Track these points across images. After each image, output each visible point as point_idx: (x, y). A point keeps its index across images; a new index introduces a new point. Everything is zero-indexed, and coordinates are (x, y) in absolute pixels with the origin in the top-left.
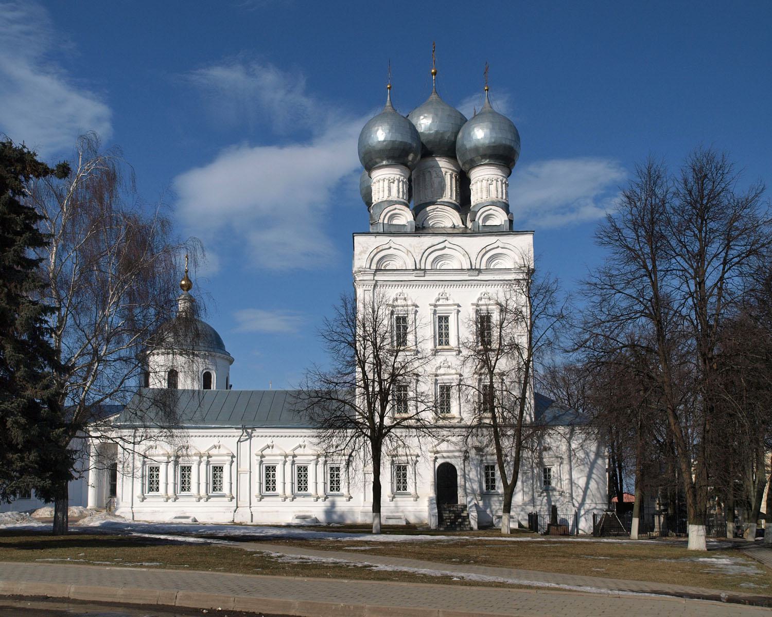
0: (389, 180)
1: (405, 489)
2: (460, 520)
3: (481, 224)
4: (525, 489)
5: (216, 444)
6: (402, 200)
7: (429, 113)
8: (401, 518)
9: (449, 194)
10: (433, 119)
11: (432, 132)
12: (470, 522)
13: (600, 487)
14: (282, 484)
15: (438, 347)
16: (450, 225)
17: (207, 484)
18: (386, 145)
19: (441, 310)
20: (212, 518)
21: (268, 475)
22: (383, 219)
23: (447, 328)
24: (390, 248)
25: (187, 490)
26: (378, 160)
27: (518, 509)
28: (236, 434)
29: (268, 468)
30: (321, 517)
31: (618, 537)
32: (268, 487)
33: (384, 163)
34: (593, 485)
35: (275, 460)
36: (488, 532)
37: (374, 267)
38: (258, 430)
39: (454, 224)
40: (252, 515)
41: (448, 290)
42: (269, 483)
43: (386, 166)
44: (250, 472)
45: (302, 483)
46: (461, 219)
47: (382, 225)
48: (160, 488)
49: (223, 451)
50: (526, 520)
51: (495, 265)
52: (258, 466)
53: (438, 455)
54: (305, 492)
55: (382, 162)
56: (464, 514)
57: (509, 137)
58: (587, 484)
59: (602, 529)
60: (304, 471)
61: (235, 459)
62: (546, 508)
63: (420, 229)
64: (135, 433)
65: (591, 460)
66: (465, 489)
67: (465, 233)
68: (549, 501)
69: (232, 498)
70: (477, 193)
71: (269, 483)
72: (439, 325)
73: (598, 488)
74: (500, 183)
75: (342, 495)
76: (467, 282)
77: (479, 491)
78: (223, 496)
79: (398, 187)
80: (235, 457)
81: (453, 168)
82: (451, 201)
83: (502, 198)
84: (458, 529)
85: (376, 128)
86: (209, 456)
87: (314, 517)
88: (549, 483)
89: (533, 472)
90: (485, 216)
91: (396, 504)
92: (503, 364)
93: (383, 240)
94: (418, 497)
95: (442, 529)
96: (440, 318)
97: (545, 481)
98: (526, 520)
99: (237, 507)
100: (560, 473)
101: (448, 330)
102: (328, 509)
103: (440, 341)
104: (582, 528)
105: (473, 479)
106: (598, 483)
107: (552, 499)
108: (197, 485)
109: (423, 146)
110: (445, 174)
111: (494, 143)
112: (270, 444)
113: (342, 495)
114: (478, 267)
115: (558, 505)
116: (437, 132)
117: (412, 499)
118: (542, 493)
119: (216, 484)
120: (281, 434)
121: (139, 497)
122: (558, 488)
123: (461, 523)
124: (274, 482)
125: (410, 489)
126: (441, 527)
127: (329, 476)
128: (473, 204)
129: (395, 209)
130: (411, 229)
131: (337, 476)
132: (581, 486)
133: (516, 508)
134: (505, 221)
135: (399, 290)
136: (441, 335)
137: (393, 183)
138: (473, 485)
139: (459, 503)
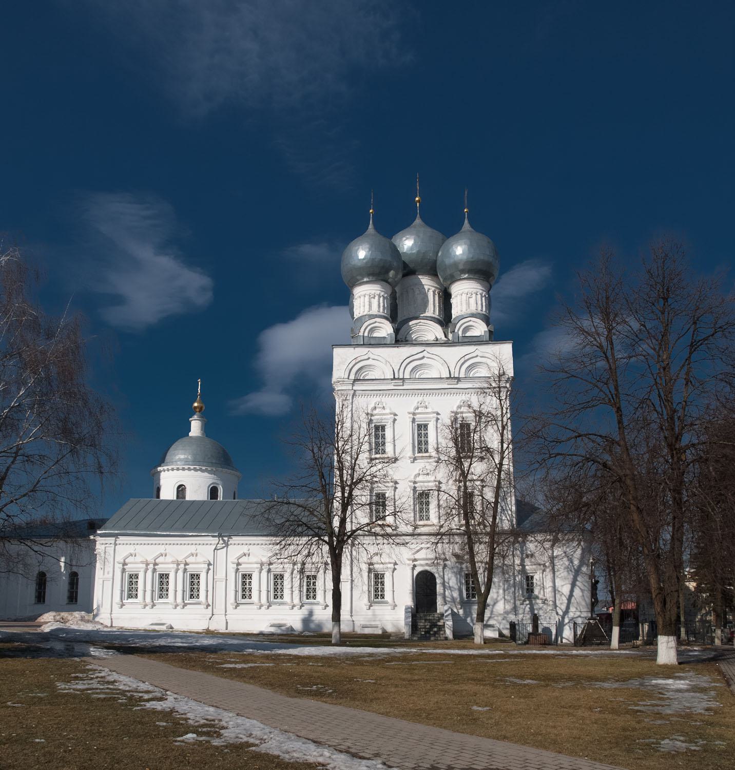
0: (370, 296)
1: (383, 598)
2: (435, 629)
3: (460, 335)
4: (506, 597)
5: (194, 552)
6: (383, 314)
7: (412, 235)
8: (377, 627)
9: (432, 309)
10: (415, 240)
11: (414, 251)
12: (445, 631)
13: (585, 595)
14: (392, 592)
15: (417, 455)
16: (433, 338)
17: (184, 591)
18: (366, 263)
19: (420, 419)
20: (187, 626)
21: (244, 583)
22: (363, 331)
23: (426, 435)
24: (369, 358)
25: (247, 597)
26: (359, 277)
27: (500, 618)
28: (213, 542)
29: (244, 576)
30: (298, 626)
31: (601, 647)
32: (244, 595)
33: (365, 280)
34: (577, 592)
35: (251, 568)
36: (462, 643)
37: (352, 377)
38: (234, 538)
39: (436, 337)
40: (227, 623)
41: (428, 399)
42: (245, 591)
43: (367, 283)
44: (226, 580)
45: (277, 591)
46: (444, 332)
47: (362, 338)
48: (138, 595)
49: (200, 559)
50: (507, 629)
51: (474, 374)
52: (234, 574)
53: (415, 563)
54: (197, 600)
55: (363, 279)
56: (440, 623)
57: (488, 253)
58: (572, 591)
59: (582, 641)
60: (381, 579)
61: (211, 567)
62: (528, 616)
63: (401, 338)
64: (116, 541)
65: (575, 567)
66: (444, 597)
67: (447, 344)
68: (532, 609)
69: (208, 605)
70: (457, 307)
71: (245, 591)
72: (418, 433)
73: (583, 596)
74: (479, 296)
75: (318, 604)
76: (446, 391)
77: (458, 599)
78: (199, 604)
79: (379, 302)
80: (211, 565)
81: (437, 286)
82: (434, 316)
83: (482, 310)
84: (432, 638)
85: (357, 248)
86: (186, 564)
87: (289, 625)
88: (532, 591)
89: (515, 579)
90: (464, 329)
91: (374, 612)
92: (478, 468)
93: (361, 352)
94: (396, 606)
95: (415, 638)
96: (419, 426)
97: (527, 589)
98: (507, 629)
99: (213, 615)
100: (543, 581)
101: (427, 438)
102: (305, 618)
103: (419, 448)
104: (566, 637)
105: (453, 587)
106: (582, 591)
107: (535, 607)
108: (258, 592)
109: (405, 265)
110: (428, 291)
111: (472, 258)
112: (246, 551)
113: (318, 604)
114: (456, 375)
115: (541, 612)
116: (418, 252)
117: (390, 607)
118: (524, 601)
119: (193, 592)
120: (254, 542)
121: (232, 604)
122: (541, 596)
123: (436, 633)
124: (315, 590)
125: (388, 596)
126: (414, 636)
127: (305, 584)
128: (453, 317)
129: (376, 322)
130: (391, 341)
131: (313, 584)
132: (565, 594)
133: (497, 616)
134: (485, 332)
135: (377, 399)
136: (420, 443)
137: (374, 298)
138: (453, 593)
139: (438, 612)
